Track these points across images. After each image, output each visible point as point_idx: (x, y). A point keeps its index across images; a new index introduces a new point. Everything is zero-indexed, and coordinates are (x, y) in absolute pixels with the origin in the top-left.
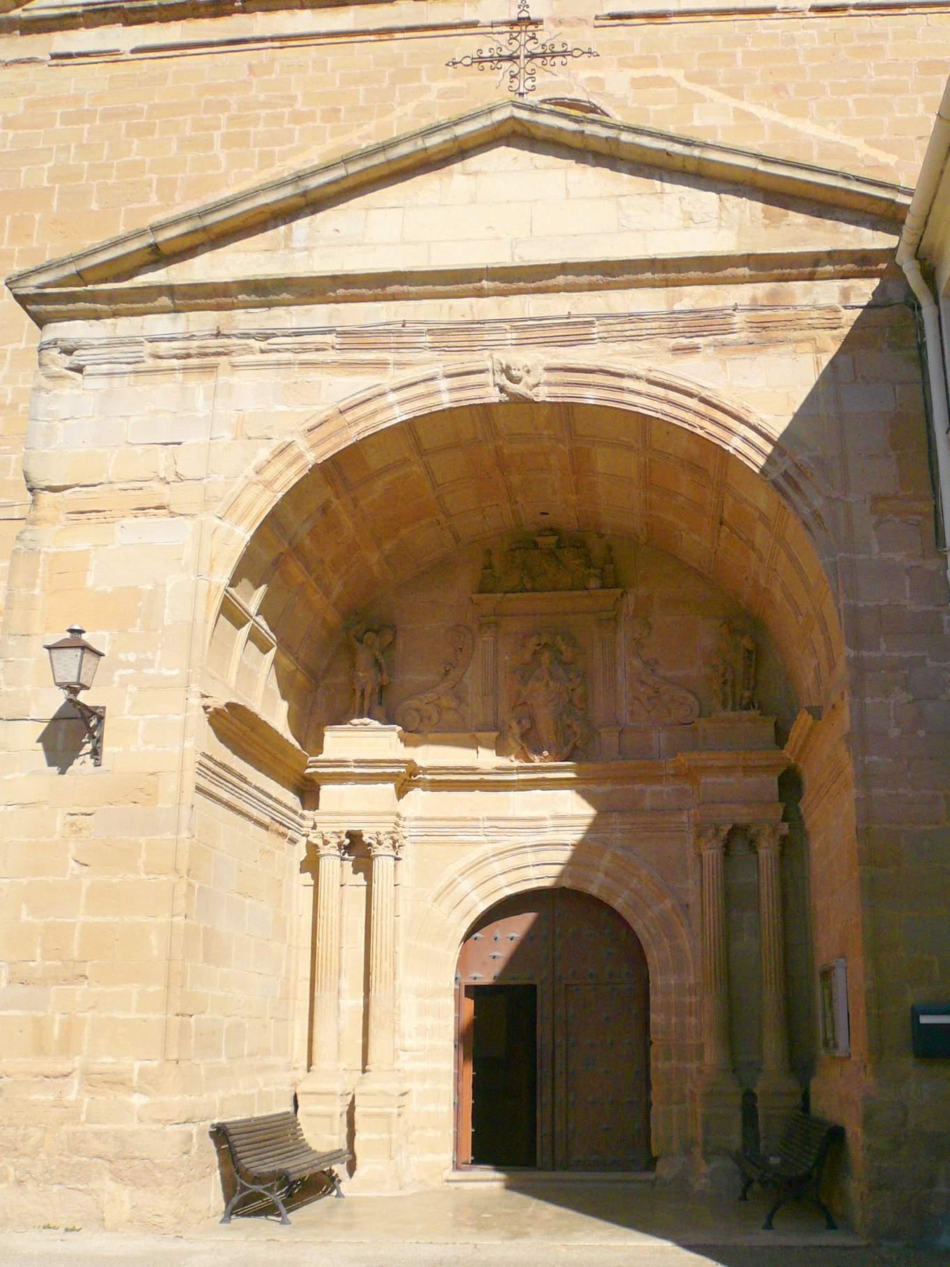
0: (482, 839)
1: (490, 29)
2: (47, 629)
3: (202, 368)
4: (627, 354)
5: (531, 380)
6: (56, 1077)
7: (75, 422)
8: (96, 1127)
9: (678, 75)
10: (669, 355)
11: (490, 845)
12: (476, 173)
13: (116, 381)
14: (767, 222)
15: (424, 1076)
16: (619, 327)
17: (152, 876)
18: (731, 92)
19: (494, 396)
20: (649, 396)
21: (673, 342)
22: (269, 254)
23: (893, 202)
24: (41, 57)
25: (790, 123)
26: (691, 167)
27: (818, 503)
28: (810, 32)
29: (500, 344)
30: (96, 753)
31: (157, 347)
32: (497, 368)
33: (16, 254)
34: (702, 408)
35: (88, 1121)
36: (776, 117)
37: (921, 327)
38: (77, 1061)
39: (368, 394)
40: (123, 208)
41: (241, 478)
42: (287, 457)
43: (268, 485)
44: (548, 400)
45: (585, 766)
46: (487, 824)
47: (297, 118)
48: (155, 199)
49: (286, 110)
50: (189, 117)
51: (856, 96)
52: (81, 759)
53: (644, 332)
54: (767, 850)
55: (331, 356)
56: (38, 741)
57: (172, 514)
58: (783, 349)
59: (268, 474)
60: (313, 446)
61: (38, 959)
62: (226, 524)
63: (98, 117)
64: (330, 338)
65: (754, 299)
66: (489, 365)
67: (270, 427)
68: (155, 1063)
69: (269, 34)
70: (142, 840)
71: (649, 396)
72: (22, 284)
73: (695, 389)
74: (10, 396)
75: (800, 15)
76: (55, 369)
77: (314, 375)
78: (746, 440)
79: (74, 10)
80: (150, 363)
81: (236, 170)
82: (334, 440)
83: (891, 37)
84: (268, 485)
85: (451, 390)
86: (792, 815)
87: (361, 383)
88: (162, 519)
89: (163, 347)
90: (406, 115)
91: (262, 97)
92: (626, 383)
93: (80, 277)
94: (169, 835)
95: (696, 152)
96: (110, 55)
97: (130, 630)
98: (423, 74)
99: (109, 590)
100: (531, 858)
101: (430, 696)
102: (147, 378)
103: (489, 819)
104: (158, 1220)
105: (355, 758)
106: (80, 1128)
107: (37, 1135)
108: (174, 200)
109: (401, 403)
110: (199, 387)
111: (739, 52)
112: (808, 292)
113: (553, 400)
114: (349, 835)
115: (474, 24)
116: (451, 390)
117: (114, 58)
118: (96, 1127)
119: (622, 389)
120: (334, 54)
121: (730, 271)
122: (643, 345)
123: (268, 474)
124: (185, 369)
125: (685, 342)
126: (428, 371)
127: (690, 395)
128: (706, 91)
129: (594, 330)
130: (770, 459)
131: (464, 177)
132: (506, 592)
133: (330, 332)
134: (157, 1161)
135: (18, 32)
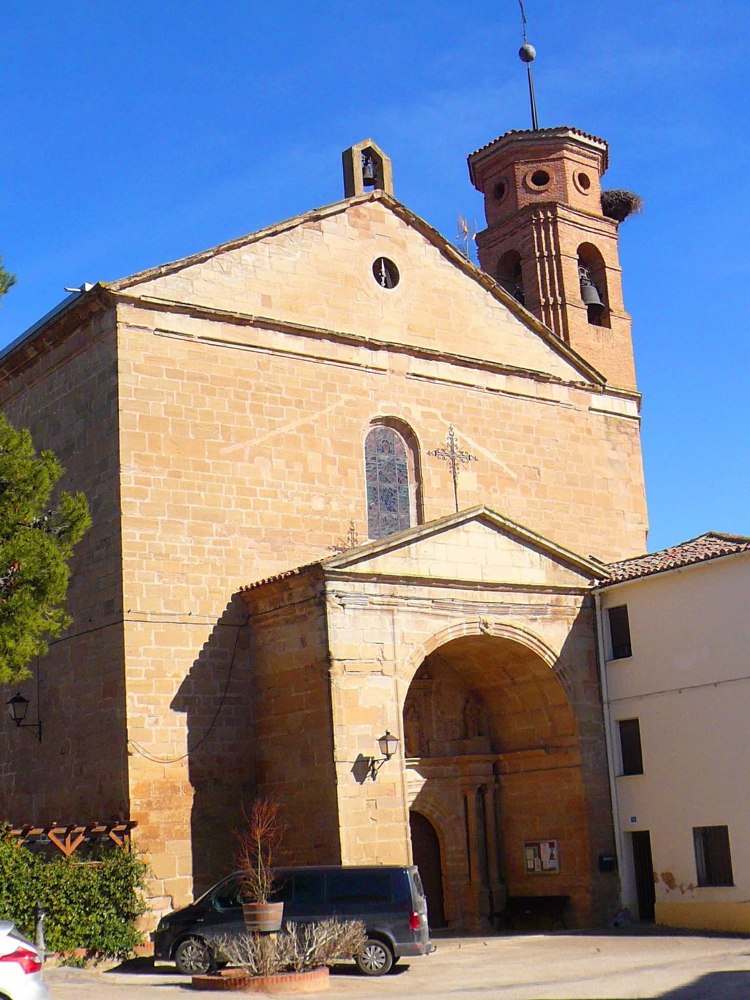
1: (364, 369)
4: (517, 620)
7: (343, 630)
10: (529, 622)
13: (357, 611)
19: (479, 633)
20: (523, 637)
22: (404, 559)
23: (591, 569)
24: (150, 327)
28: (486, 400)
31: (373, 599)
34: (538, 643)
37: (595, 616)
45: (425, 760)
47: (285, 402)
52: (367, 778)
56: (351, 771)
58: (560, 622)
71: (523, 637)
72: (327, 566)
73: (537, 637)
74: (164, 549)
77: (425, 618)
78: (550, 657)
79: (171, 303)
80: (369, 606)
83: (514, 410)
89: (376, 599)
92: (517, 631)
95: (538, 539)
99: (368, 707)
115: (359, 365)
119: (515, 633)
121: (547, 591)
124: (382, 610)
127: (535, 638)
130: (555, 663)
135: (133, 305)
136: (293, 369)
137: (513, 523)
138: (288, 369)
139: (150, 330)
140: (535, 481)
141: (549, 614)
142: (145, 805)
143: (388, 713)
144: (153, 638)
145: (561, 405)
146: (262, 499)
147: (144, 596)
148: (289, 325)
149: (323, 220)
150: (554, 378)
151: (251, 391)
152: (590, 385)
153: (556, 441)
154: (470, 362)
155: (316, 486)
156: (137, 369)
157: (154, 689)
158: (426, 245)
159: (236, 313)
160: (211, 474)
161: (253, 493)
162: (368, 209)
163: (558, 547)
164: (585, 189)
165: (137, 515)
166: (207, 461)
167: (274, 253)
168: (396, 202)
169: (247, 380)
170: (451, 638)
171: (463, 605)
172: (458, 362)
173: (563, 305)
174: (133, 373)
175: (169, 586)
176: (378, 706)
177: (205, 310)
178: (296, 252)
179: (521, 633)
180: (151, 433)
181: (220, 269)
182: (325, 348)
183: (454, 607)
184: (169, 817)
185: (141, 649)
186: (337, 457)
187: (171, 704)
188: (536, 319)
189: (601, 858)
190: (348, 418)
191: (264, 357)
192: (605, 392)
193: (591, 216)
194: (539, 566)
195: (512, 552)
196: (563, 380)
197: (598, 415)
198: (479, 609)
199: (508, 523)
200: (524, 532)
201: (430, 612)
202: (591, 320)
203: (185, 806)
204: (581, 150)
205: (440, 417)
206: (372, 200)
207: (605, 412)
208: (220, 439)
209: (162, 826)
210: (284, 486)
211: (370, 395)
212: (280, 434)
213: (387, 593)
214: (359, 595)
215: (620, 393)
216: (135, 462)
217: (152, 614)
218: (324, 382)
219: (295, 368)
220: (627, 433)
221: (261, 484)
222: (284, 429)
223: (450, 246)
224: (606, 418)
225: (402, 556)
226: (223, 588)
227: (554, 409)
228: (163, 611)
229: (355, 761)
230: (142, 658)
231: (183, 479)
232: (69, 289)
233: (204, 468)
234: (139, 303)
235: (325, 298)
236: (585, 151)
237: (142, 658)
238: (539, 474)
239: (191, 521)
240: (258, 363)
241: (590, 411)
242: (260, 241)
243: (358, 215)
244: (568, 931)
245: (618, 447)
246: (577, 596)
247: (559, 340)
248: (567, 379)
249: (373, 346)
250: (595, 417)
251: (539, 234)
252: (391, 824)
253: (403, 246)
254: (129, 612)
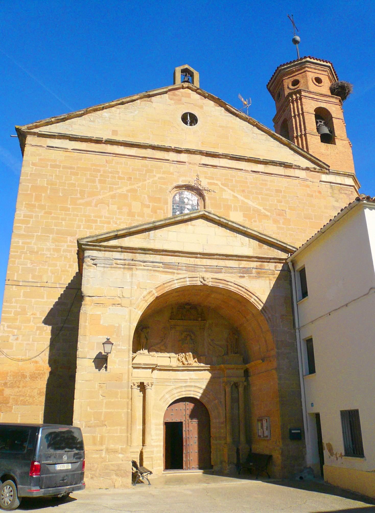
0: (172, 384)
1: (172, 162)
2: (90, 334)
3: (129, 268)
5: (208, 281)
6: (99, 451)
7: (95, 279)
8: (111, 463)
9: (219, 183)
10: (239, 277)
11: (174, 386)
12: (194, 225)
13: (105, 269)
14: (259, 247)
15: (157, 446)
16: (228, 270)
17: (122, 400)
18: (232, 190)
19: (199, 284)
21: (239, 275)
22: (144, 240)
24: (43, 146)
25: (246, 201)
26: (243, 232)
27: (270, 315)
28: (251, 177)
29: (202, 271)
30: (106, 367)
32: (201, 277)
33: (37, 205)
34: (245, 291)
35: (109, 461)
36: (242, 198)
37: (291, 276)
38: (104, 447)
39: (170, 280)
40: (70, 197)
41: (140, 299)
42: (151, 295)
43: (146, 301)
44: (211, 285)
46: (173, 380)
47: (120, 178)
48: (79, 195)
49: (117, 175)
50: (89, 172)
51: (261, 196)
53: (234, 272)
54: (241, 389)
55: (161, 269)
57: (122, 306)
58: (263, 279)
59: (146, 298)
60: (157, 292)
61: (93, 421)
62: (136, 310)
63: (61, 167)
64: (161, 265)
65: (257, 266)
66: (199, 276)
67: (146, 286)
68: (125, 446)
69: (112, 152)
70: (119, 390)
72: (82, 241)
73: (244, 287)
75: (248, 172)
76: (89, 264)
77: (157, 274)
78: (255, 299)
79: (55, 134)
80: (115, 265)
81: (103, 191)
82: (162, 291)
84: (146, 301)
85: (189, 281)
86: (247, 380)
87: (167, 277)
88: (119, 308)
90: (150, 182)
91: (110, 170)
92: (229, 283)
93: (97, 241)
94: (126, 389)
95: (245, 229)
96: (66, 150)
97: (113, 336)
98: (154, 171)
99: (107, 325)
100: (184, 389)
101: (159, 346)
102: (114, 269)
103: (174, 379)
104: (127, 485)
105: (143, 363)
106: (107, 463)
107: (96, 466)
108: (84, 197)
109: (177, 283)
110: (128, 273)
111: (234, 179)
112: (268, 266)
113: (212, 286)
114: (141, 383)
115: (168, 160)
116: (189, 281)
117: (66, 150)
118: (111, 463)
120: (130, 161)
122: (233, 275)
123: (146, 298)
124: (124, 268)
125: (242, 275)
126: (185, 276)
127: (243, 288)
128: (225, 188)
129: (223, 270)
131: (191, 226)
132: (178, 320)
133: (161, 263)
134: (127, 470)
136: (127, 163)
137: (225, 219)
138: (124, 163)
139: (44, 147)
140: (283, 217)
141: (254, 273)
142: (3, 385)
143: (122, 330)
144: (22, 294)
145: (300, 179)
146: (101, 225)
147: (20, 272)
148: (125, 142)
149: (153, 98)
150: (295, 165)
151: (100, 174)
152: (320, 169)
153: (298, 197)
154: (239, 158)
155: (136, 218)
156: (34, 164)
157: (18, 321)
158: (215, 107)
159: (93, 137)
160: (70, 212)
161: (95, 222)
162: (181, 92)
163: (260, 233)
164: (319, 84)
165: (22, 232)
166: (69, 206)
167: (122, 112)
168: (197, 88)
169: (98, 168)
170: (177, 286)
171: (185, 266)
172: (231, 158)
173: (305, 135)
174: (31, 166)
175: (36, 268)
176: (116, 325)
177: (75, 136)
178: (136, 111)
179: (232, 285)
180: (37, 193)
181: (89, 120)
182: (149, 153)
183: (179, 267)
184: (17, 392)
185: (14, 300)
186: (151, 204)
188: (283, 138)
189: (290, 430)
190: (159, 185)
191: (110, 158)
192: (330, 173)
193: (322, 95)
194: (248, 246)
195: (227, 237)
196: (301, 166)
197: (326, 184)
198: (198, 269)
199: (222, 220)
200: (234, 225)
201: (161, 270)
202: (322, 141)
203: (29, 387)
205: (220, 185)
206: (183, 88)
207: (330, 183)
208: (79, 195)
209: (12, 397)
210: (115, 218)
211: (175, 175)
212: (116, 193)
213: (130, 258)
214: (106, 259)
215: (340, 173)
216: (25, 207)
217: (23, 282)
218: (146, 169)
219: (129, 162)
220: (346, 194)
221: (100, 217)
222: (119, 191)
223: (229, 105)
224: (331, 186)
225: (143, 238)
226: (70, 270)
227: (297, 181)
228: (30, 280)
229: (94, 358)
230: (13, 304)
231: (53, 215)
232: (12, 136)
233: (68, 209)
234: (34, 134)
235: (151, 131)
237: (13, 304)
238: (286, 213)
239: (55, 235)
240: (106, 160)
241: (321, 183)
242: (115, 107)
243: (174, 95)
244: (269, 480)
245: (340, 200)
246: (277, 264)
247: (304, 151)
248: (304, 166)
249: (179, 151)
250: (324, 186)
251: (293, 106)
252: (117, 400)
253: (201, 107)
254: (9, 280)
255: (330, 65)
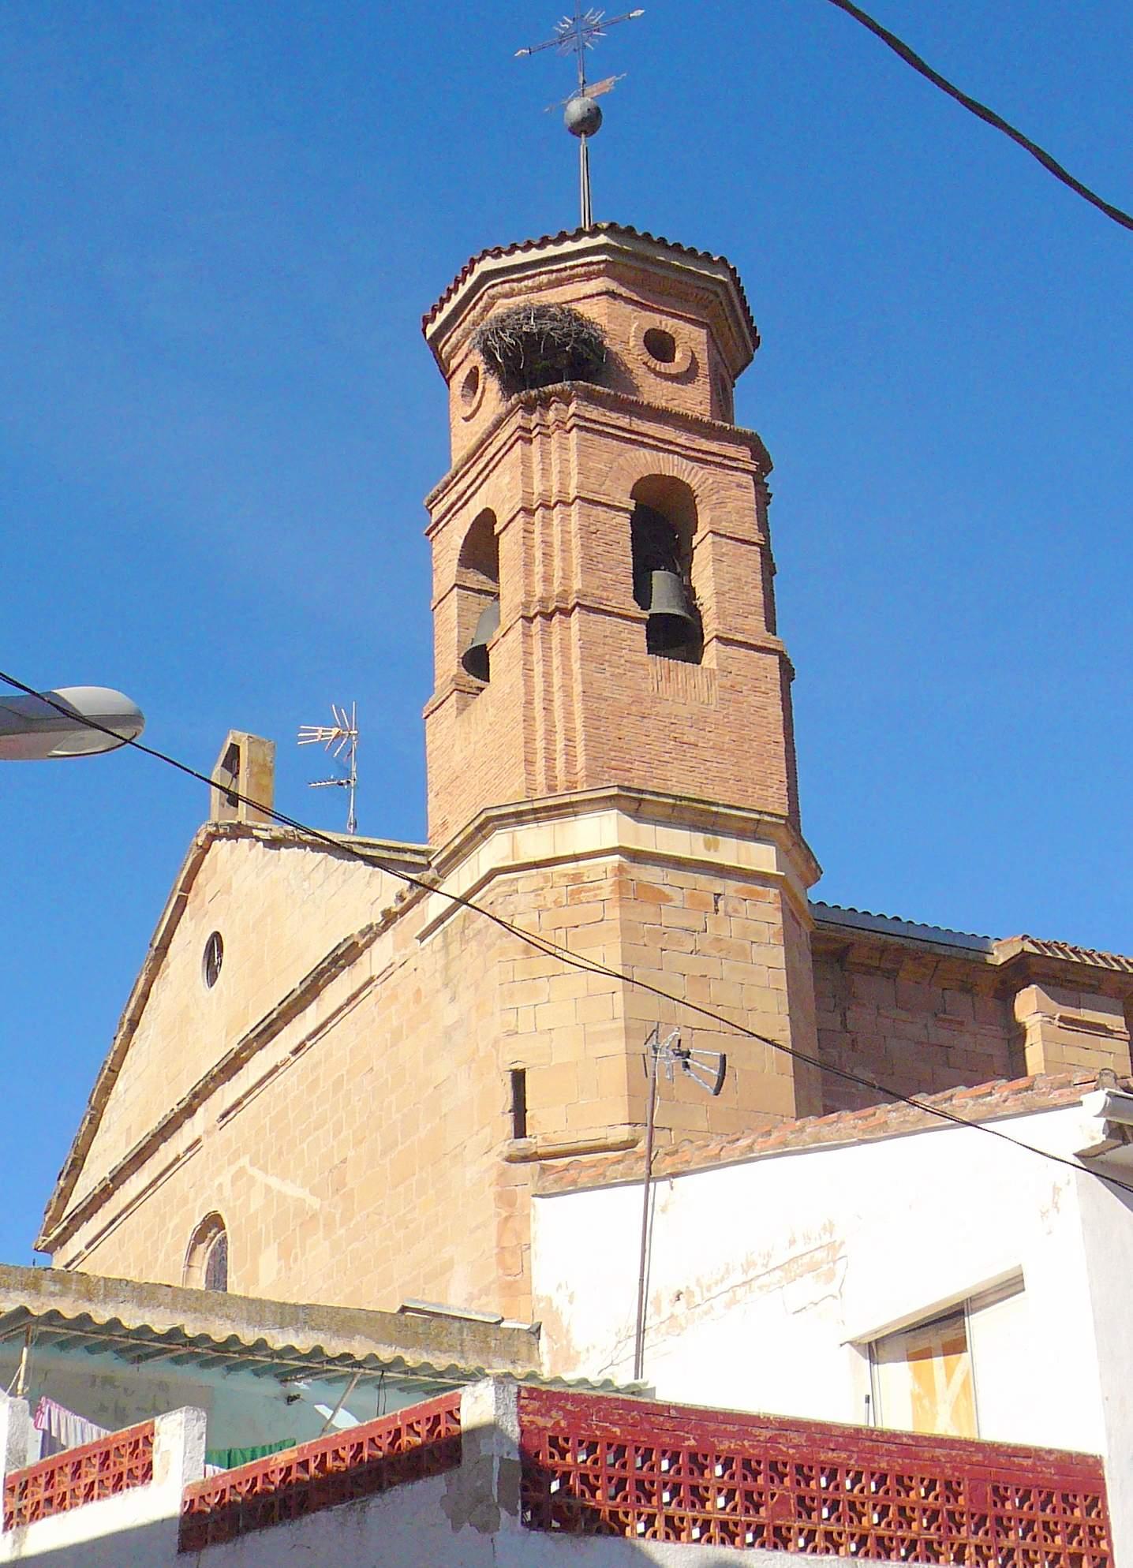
150: (363, 933)
187: (238, 1338)
204: (463, 325)
236: (469, 318)
255: (489, 264)
